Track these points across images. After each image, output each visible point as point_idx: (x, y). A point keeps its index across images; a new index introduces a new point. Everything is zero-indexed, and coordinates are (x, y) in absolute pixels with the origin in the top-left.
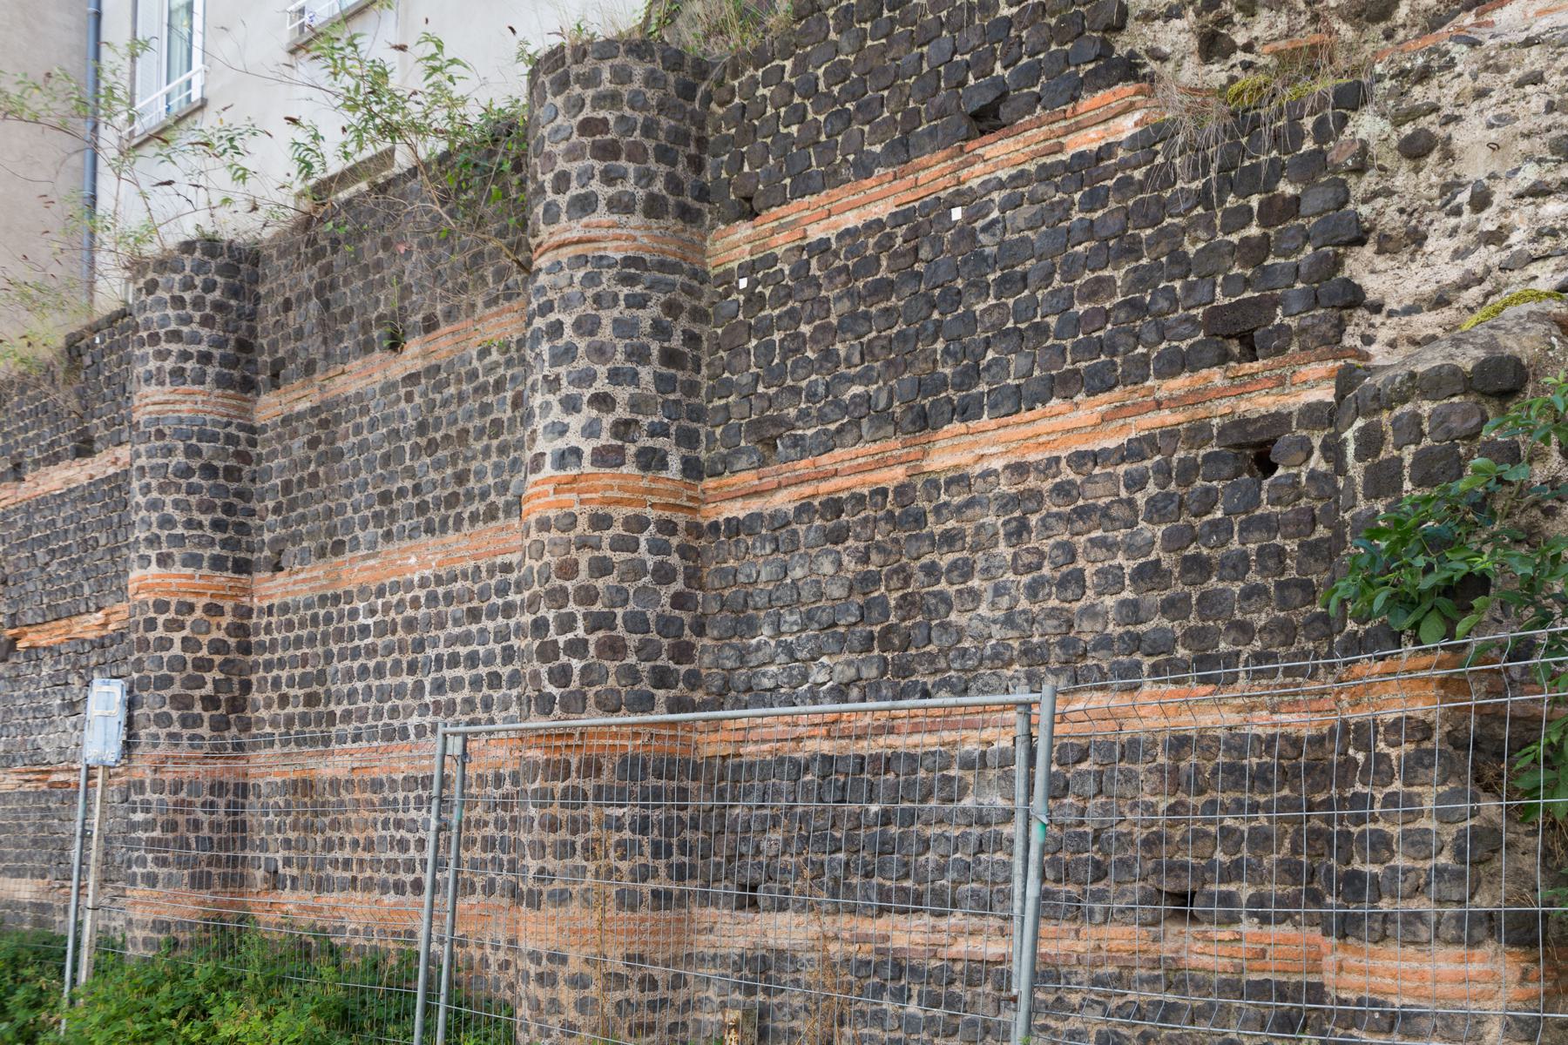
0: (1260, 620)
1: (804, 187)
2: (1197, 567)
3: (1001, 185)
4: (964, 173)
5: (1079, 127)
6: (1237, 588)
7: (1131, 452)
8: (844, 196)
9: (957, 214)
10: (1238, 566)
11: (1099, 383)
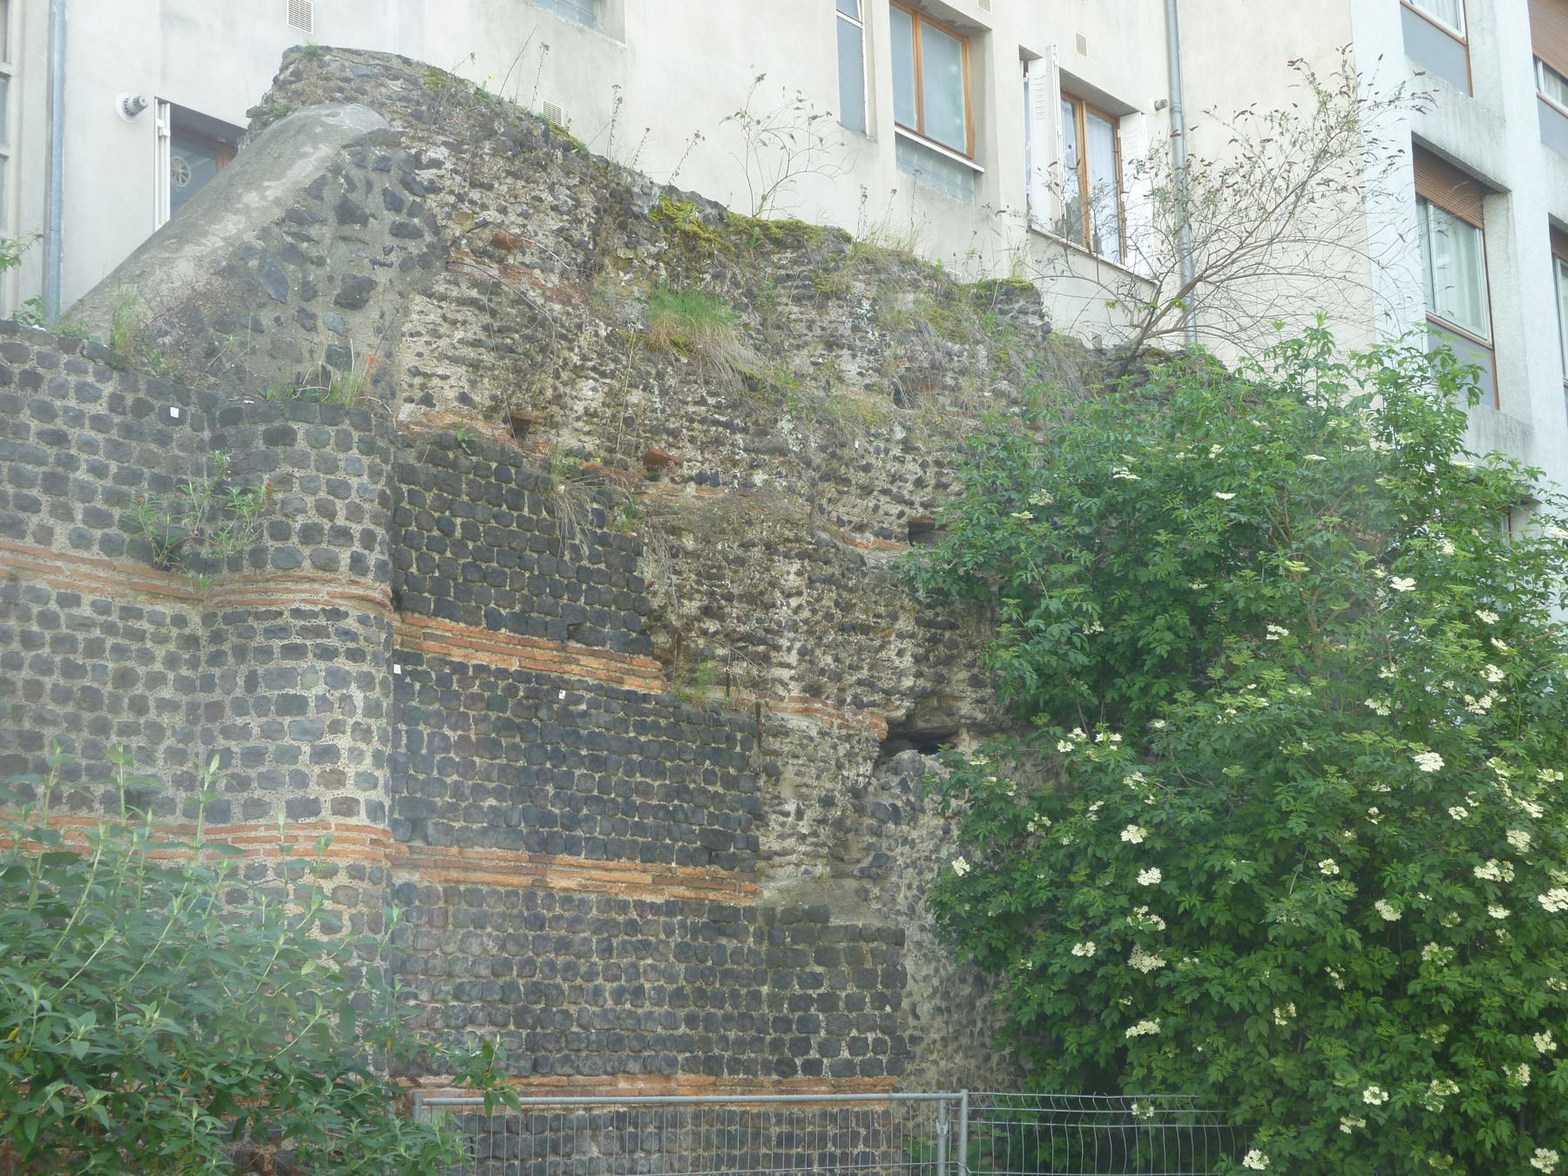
0: (732, 1035)
1: (444, 610)
2: (701, 993)
3: (589, 688)
4: (566, 667)
5: (633, 673)
6: (720, 1013)
7: (671, 908)
8: (477, 633)
9: (562, 695)
10: (718, 1000)
11: (648, 854)
